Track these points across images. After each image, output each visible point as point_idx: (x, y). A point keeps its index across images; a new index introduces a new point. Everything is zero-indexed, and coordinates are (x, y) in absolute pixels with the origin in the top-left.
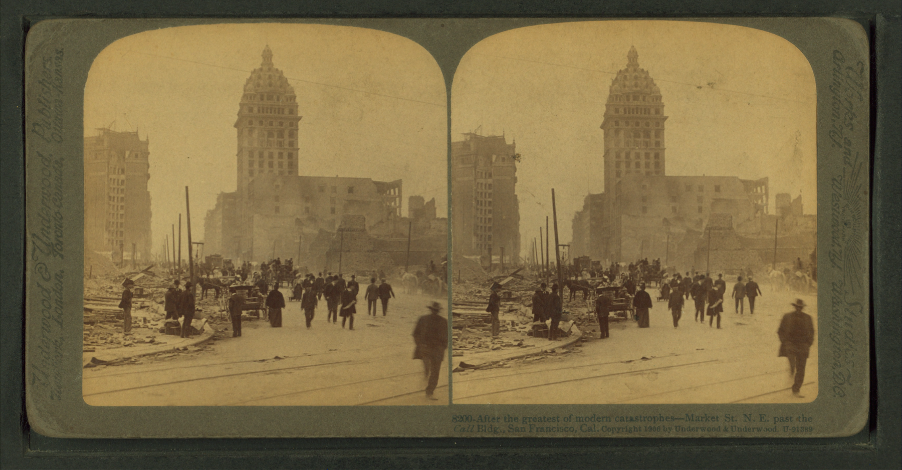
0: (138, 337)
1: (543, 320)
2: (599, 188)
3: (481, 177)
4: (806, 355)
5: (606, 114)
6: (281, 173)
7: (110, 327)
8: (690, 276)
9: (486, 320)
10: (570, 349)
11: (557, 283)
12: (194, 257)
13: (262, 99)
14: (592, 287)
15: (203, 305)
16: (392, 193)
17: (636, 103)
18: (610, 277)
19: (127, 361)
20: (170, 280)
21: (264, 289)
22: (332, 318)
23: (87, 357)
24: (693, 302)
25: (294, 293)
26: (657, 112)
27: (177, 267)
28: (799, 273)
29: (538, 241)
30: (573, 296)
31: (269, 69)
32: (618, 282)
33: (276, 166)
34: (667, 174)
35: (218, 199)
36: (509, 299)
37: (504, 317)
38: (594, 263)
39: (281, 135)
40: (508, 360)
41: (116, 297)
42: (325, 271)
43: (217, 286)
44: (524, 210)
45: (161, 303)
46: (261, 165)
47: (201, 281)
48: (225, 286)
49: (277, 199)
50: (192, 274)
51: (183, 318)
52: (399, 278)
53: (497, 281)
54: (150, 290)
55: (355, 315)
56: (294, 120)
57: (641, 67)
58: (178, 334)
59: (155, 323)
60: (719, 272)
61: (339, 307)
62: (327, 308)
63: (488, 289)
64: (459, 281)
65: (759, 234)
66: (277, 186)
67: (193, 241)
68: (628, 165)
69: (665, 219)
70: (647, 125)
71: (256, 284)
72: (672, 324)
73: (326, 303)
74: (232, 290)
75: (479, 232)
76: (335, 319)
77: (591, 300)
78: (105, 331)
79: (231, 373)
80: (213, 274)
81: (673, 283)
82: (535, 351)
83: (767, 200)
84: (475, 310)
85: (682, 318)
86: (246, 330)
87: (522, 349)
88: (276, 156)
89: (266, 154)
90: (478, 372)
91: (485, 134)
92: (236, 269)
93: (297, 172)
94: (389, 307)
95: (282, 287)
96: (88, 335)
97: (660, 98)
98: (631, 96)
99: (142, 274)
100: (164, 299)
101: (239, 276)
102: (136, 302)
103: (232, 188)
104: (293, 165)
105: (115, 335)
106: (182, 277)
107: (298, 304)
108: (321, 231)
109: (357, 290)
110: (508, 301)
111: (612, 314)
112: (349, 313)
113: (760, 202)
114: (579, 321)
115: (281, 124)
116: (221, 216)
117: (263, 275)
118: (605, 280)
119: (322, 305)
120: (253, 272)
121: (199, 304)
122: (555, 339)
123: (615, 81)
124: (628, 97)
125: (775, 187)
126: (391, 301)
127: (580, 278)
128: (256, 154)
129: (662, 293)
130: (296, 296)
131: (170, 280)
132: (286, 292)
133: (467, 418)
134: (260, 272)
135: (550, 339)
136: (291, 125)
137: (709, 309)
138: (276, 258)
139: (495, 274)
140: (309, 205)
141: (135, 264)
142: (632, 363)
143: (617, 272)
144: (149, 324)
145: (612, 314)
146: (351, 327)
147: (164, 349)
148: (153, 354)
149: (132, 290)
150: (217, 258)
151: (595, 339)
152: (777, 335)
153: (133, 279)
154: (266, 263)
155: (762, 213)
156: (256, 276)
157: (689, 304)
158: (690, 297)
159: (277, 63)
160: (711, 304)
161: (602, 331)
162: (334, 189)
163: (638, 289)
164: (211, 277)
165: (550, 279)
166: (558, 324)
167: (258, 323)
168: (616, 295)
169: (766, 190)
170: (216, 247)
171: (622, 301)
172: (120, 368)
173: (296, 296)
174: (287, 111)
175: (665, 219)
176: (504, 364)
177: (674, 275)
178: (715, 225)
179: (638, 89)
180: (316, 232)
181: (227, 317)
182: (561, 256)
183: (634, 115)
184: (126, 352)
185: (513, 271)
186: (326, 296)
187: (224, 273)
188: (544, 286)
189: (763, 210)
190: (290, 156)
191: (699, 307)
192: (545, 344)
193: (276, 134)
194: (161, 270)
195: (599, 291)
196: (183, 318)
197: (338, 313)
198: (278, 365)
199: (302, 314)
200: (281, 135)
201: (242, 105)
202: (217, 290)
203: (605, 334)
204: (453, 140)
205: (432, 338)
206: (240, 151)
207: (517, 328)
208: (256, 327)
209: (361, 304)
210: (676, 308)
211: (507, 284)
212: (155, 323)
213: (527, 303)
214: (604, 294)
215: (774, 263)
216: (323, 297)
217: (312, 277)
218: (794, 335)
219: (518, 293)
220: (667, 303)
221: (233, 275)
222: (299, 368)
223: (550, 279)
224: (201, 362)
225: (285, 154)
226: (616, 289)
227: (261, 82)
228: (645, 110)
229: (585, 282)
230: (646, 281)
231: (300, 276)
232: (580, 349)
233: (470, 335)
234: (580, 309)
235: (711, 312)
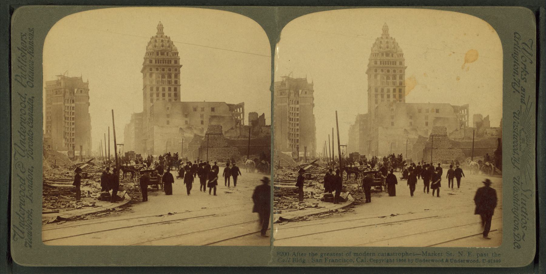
1: (331, 192)
2: (364, 111)
3: (292, 104)
4: (492, 214)
5: (369, 65)
6: (170, 100)
7: (67, 198)
8: (421, 164)
9: (295, 191)
10: (347, 209)
11: (339, 168)
12: (118, 153)
13: (158, 55)
14: (361, 171)
15: (124, 182)
16: (463, 113)
17: (162, 57)
19: (302, 219)
20: (104, 167)
21: (385, 173)
22: (203, 189)
23: (276, 217)
24: (423, 181)
25: (179, 173)
26: (176, 62)
27: (108, 160)
28: (487, 163)
29: (327, 143)
30: (125, 176)
31: (162, 37)
32: (376, 168)
33: (167, 95)
35: (132, 117)
37: (306, 190)
38: (137, 156)
39: (170, 76)
40: (309, 216)
41: (71, 178)
42: (198, 160)
43: (132, 170)
44: (319, 124)
45: (99, 182)
46: (158, 95)
47: (123, 168)
48: (137, 170)
49: (168, 116)
51: (112, 190)
52: (468, 165)
53: (302, 167)
54: (91, 174)
55: (440, 188)
57: (165, 35)
58: (332, 202)
59: (318, 195)
61: (207, 181)
62: (199, 183)
63: (297, 172)
64: (279, 167)
65: (239, 137)
66: (168, 108)
67: (341, 144)
68: (382, 96)
70: (394, 71)
71: (380, 170)
72: (410, 194)
73: (199, 179)
74: (142, 173)
75: (291, 138)
76: (428, 191)
77: (360, 180)
79: (142, 224)
80: (130, 163)
81: (410, 169)
82: (326, 210)
83: (468, 117)
84: (289, 185)
85: (415, 191)
86: (373, 199)
87: (94, 208)
88: (167, 90)
90: (290, 223)
91: (295, 77)
92: (368, 161)
93: (404, 101)
94: (461, 183)
95: (172, 170)
96: (277, 203)
97: (402, 55)
98: (160, 53)
99: (87, 165)
100: (100, 179)
101: (145, 164)
102: (84, 181)
103: (140, 110)
104: (177, 95)
105: (294, 203)
106: (111, 165)
107: (182, 180)
108: (196, 135)
109: (442, 172)
111: (372, 188)
112: (436, 186)
113: (239, 117)
114: (353, 192)
115: (170, 70)
116: (134, 128)
117: (160, 163)
118: (369, 167)
119: (197, 180)
120: (154, 162)
121: (122, 182)
122: (338, 203)
123: (374, 45)
124: (383, 54)
125: (473, 111)
126: (462, 179)
127: (353, 166)
128: (155, 89)
129: (403, 175)
130: (181, 175)
131: (104, 167)
132: (175, 173)
133: (286, 254)
134: (158, 162)
135: (335, 203)
138: (168, 152)
140: (187, 119)
142: (162, 217)
143: (152, 161)
144: (91, 195)
145: (372, 188)
146: (438, 196)
147: (100, 210)
148: (317, 214)
149: (80, 174)
150: (132, 153)
152: (474, 201)
153: (82, 167)
154: (386, 157)
155: (465, 127)
156: (156, 164)
157: (420, 182)
158: (421, 178)
159: (166, 32)
160: (433, 182)
161: (366, 198)
162: (427, 111)
163: (389, 172)
164: (129, 165)
165: (335, 167)
166: (340, 194)
167: (157, 192)
168: (376, 176)
169: (467, 112)
170: (357, 148)
172: (74, 222)
173: (181, 175)
174: (173, 62)
175: (181, 129)
176: (306, 218)
177: (411, 164)
178: (436, 133)
179: (389, 49)
180: (417, 137)
181: (139, 189)
182: (341, 152)
183: (387, 67)
184: (300, 213)
185: (88, 160)
186: (199, 175)
187: (137, 162)
188: (331, 171)
190: (175, 89)
191: (426, 184)
192: (109, 205)
193: (166, 76)
194: (322, 162)
195: (365, 174)
196: (112, 190)
197: (430, 187)
200: (170, 76)
201: (370, 60)
202: (133, 173)
203: (368, 200)
205: (262, 201)
208: (380, 196)
209: (221, 180)
210: (189, 183)
211: (309, 169)
212: (318, 195)
213: (321, 181)
214: (368, 175)
215: (472, 157)
216: (197, 176)
217: (191, 164)
218: (485, 202)
219: (315, 175)
220: (407, 181)
221: (142, 163)
222: (183, 220)
223: (335, 167)
224: (344, 219)
225: (173, 89)
227: (157, 44)
228: (388, 62)
230: (394, 168)
231: (183, 163)
232: (353, 209)
233: (285, 201)
234: (353, 185)
235: (434, 187)
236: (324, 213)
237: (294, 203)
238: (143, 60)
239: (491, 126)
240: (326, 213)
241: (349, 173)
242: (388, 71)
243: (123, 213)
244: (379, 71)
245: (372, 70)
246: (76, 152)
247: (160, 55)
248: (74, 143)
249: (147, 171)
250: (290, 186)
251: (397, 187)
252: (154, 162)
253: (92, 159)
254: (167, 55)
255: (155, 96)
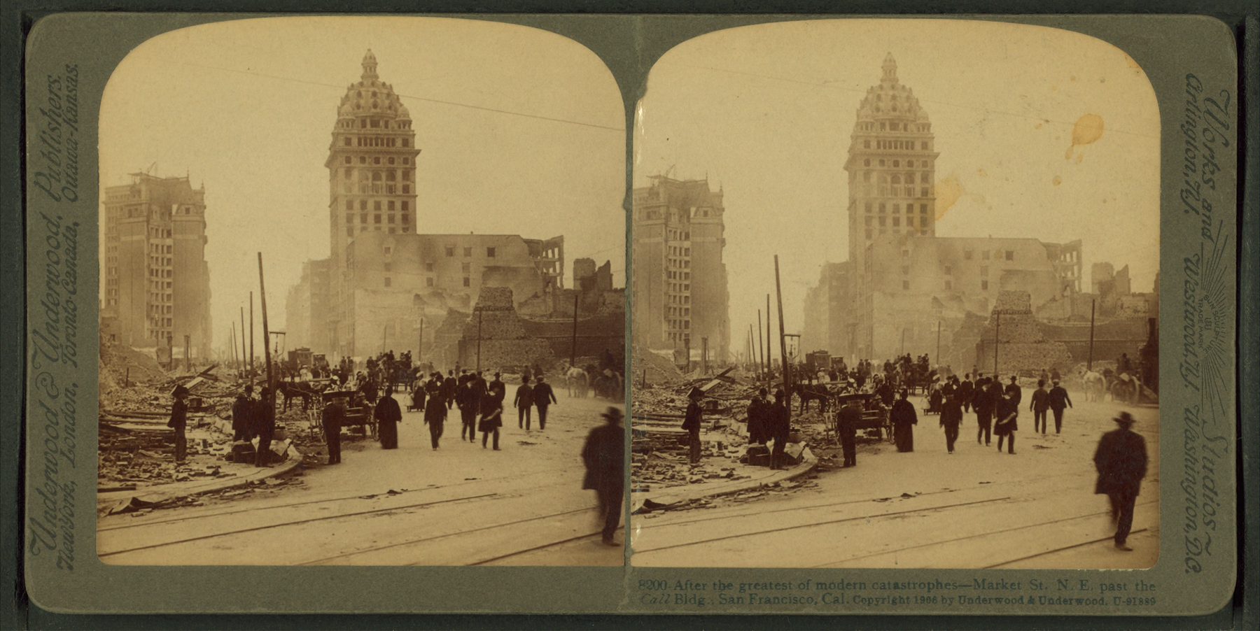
0: (195, 467)
1: (763, 442)
2: (841, 255)
4: (1135, 492)
6: (392, 231)
7: (156, 455)
8: (971, 379)
9: (681, 439)
10: (801, 481)
11: (782, 388)
13: (364, 126)
14: (832, 395)
15: (286, 420)
16: (1068, 259)
17: (374, 130)
18: (340, 376)
19: (696, 504)
20: (240, 386)
21: (888, 398)
23: (638, 500)
24: (975, 416)
25: (414, 399)
27: (248, 368)
28: (1125, 376)
29: (756, 329)
31: (373, 84)
32: (868, 387)
34: (420, 231)
35: (304, 269)
36: (715, 411)
37: (707, 437)
38: (316, 359)
39: (392, 176)
40: (713, 497)
41: (164, 411)
42: (975, 371)
43: (305, 391)
44: (735, 286)
45: (228, 418)
47: (283, 386)
48: (316, 392)
50: (786, 377)
51: (258, 438)
53: (697, 385)
54: (211, 401)
55: (1016, 433)
56: (409, 155)
57: (381, 80)
58: (766, 465)
60: (1010, 375)
61: (478, 418)
62: (460, 420)
63: (684, 397)
64: (644, 386)
65: (1069, 320)
67: (786, 332)
68: (882, 221)
69: (417, 296)
70: (910, 164)
71: (877, 392)
72: (945, 447)
73: (459, 412)
74: (327, 398)
76: (988, 440)
77: (830, 414)
78: (150, 461)
80: (300, 375)
81: (947, 389)
82: (752, 485)
83: (1080, 270)
84: (667, 426)
86: (862, 457)
88: (385, 206)
89: (370, 205)
90: (670, 514)
93: (933, 232)
95: (397, 391)
96: (640, 468)
97: (927, 126)
99: (200, 379)
100: (231, 413)
101: (336, 378)
102: (193, 418)
103: (324, 253)
104: (408, 220)
105: (678, 468)
106: (256, 381)
107: (420, 416)
110: (713, 414)
113: (551, 270)
114: (814, 443)
115: (392, 161)
116: (308, 294)
118: (851, 385)
119: (454, 415)
120: (356, 372)
121: (281, 419)
122: (779, 468)
123: (864, 103)
124: (883, 125)
126: (1067, 411)
127: (815, 382)
128: (357, 205)
129: (931, 403)
130: (417, 404)
131: (240, 386)
132: (403, 399)
133: (660, 585)
134: (365, 372)
135: (772, 468)
136: (406, 161)
137: (997, 425)
138: (387, 351)
139: (695, 375)
140: (433, 275)
141: (707, 366)
142: (374, 500)
143: (350, 370)
145: (860, 433)
146: (1011, 451)
148: (732, 494)
149: (186, 402)
150: (305, 353)
151: (319, 466)
153: (188, 386)
155: (1072, 292)
156: (361, 378)
157: (970, 420)
158: (971, 409)
160: (1000, 420)
161: (845, 456)
162: (986, 256)
163: (897, 397)
164: (297, 380)
165: (773, 384)
166: (784, 447)
167: (880, 446)
168: (867, 406)
169: (1079, 257)
170: (823, 340)
171: (874, 414)
172: (171, 512)
173: (417, 404)
174: (399, 143)
175: (417, 296)
176: (707, 503)
177: (949, 378)
178: (1007, 307)
181: (320, 436)
182: (788, 351)
183: (894, 153)
184: (693, 491)
185: (202, 369)
186: (458, 404)
187: (316, 374)
188: (764, 393)
189: (555, 282)
190: (405, 206)
191: (984, 423)
192: (251, 473)
193: (384, 176)
195: (843, 400)
196: (258, 438)
197: (477, 427)
198: (394, 502)
199: (426, 429)
200: (392, 176)
201: (854, 138)
202: (823, 402)
203: (850, 462)
204: (636, 184)
205: (605, 462)
206: (334, 200)
207: (725, 451)
208: (877, 452)
210: (436, 422)
211: (712, 390)
213: (740, 417)
214: (849, 404)
215: (1090, 362)
216: (454, 405)
218: (1119, 465)
219: (727, 403)
220: (938, 417)
221: (328, 376)
223: (773, 384)
225: (398, 205)
226: (349, 393)
227: (362, 102)
228: (896, 142)
229: (822, 388)
230: (909, 387)
231: (422, 376)
233: (659, 462)
234: (814, 426)
235: (1001, 431)
236: (746, 490)
237: (678, 468)
238: (331, 139)
239: (1133, 291)
240: (753, 490)
241: (805, 398)
242: (896, 164)
243: (284, 491)
244: (875, 163)
245: (860, 162)
246: (175, 350)
247: (369, 126)
248: (170, 329)
249: (339, 394)
250: (669, 429)
251: (916, 430)
252: (356, 372)
253: (213, 367)
254: (387, 127)
255: (357, 221)
